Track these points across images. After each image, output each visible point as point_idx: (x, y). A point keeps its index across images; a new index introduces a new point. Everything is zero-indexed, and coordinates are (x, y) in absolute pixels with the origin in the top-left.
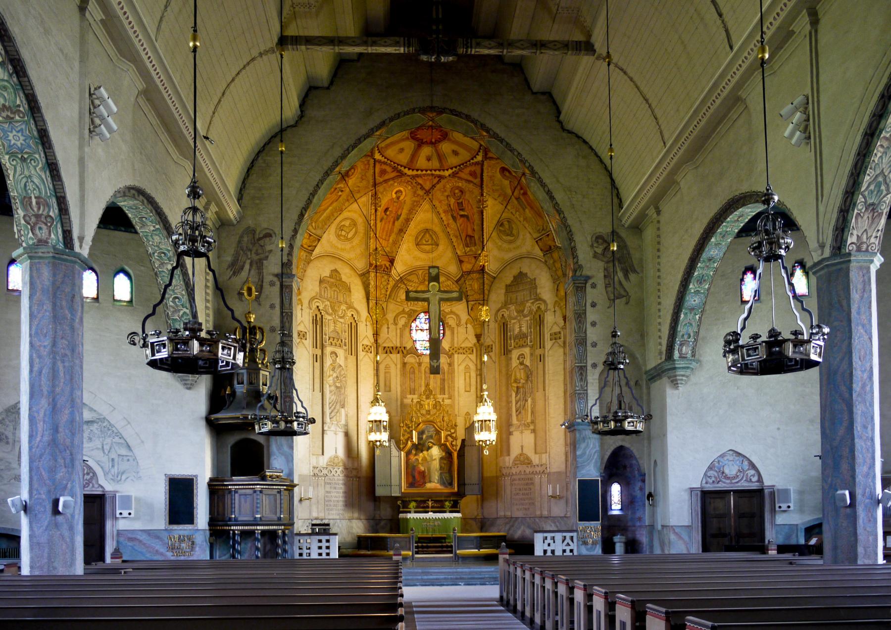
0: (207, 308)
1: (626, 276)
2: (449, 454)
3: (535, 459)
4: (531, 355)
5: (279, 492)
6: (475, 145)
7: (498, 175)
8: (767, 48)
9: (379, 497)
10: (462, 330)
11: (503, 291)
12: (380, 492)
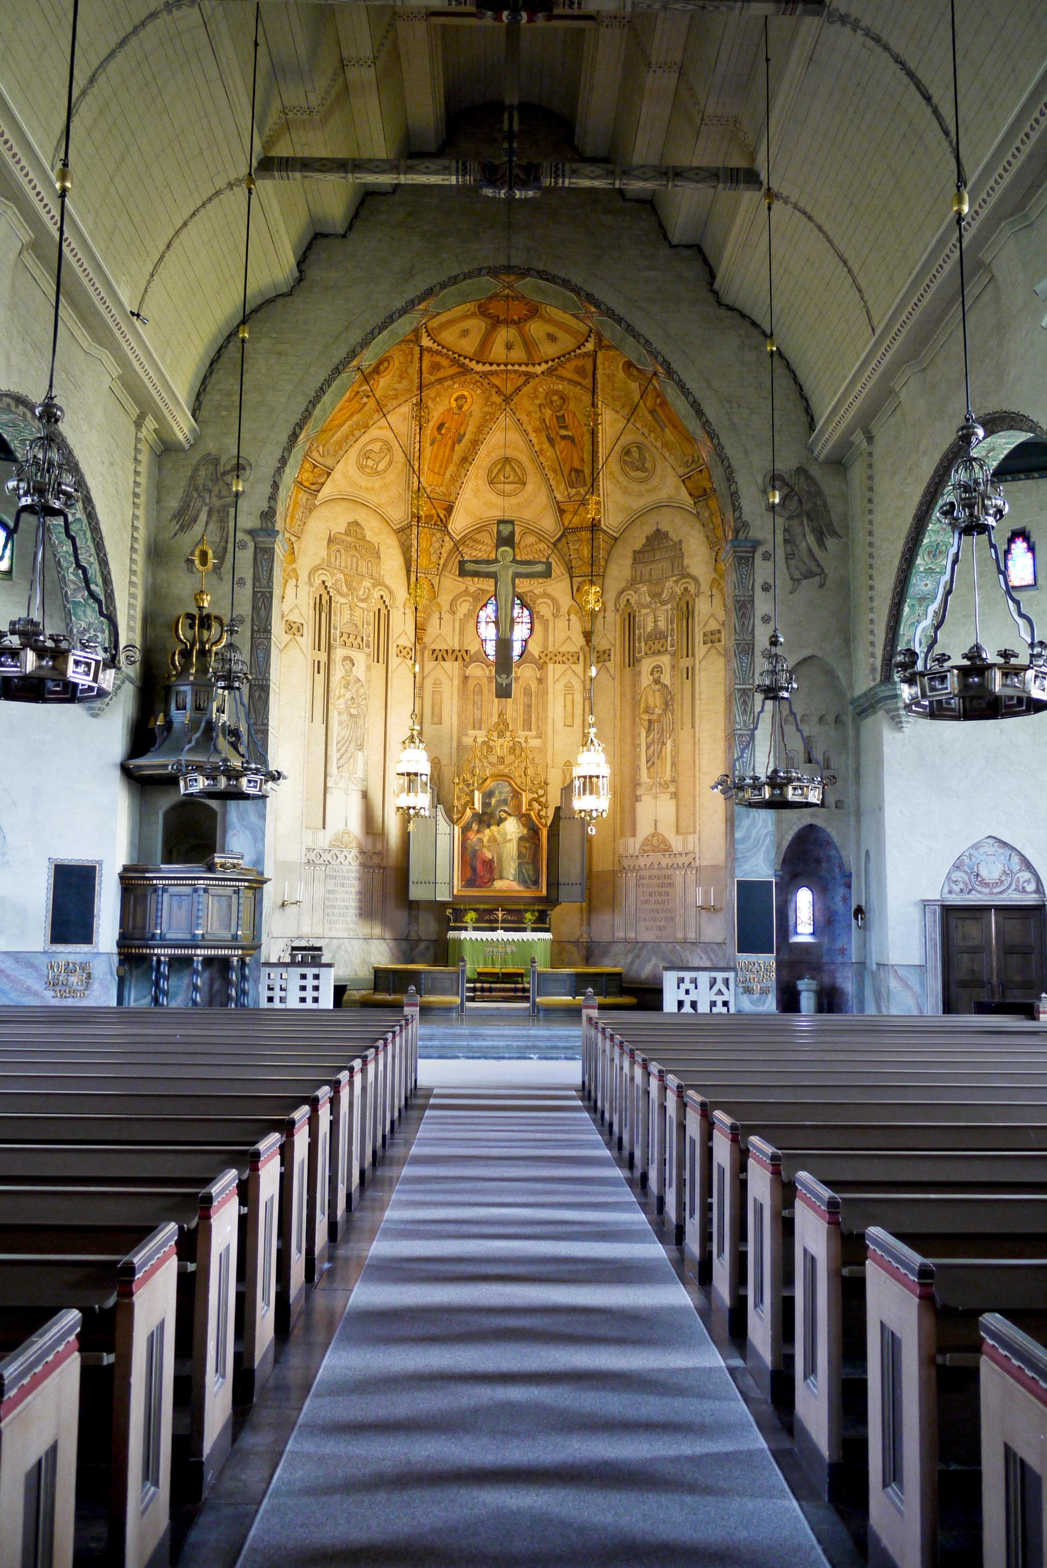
0: (132, 583)
1: (821, 544)
2: (533, 831)
3: (676, 843)
4: (673, 667)
5: (237, 892)
6: (582, 328)
7: (621, 375)
8: (966, 197)
9: (418, 902)
10: (562, 623)
11: (630, 561)
12: (416, 893)
